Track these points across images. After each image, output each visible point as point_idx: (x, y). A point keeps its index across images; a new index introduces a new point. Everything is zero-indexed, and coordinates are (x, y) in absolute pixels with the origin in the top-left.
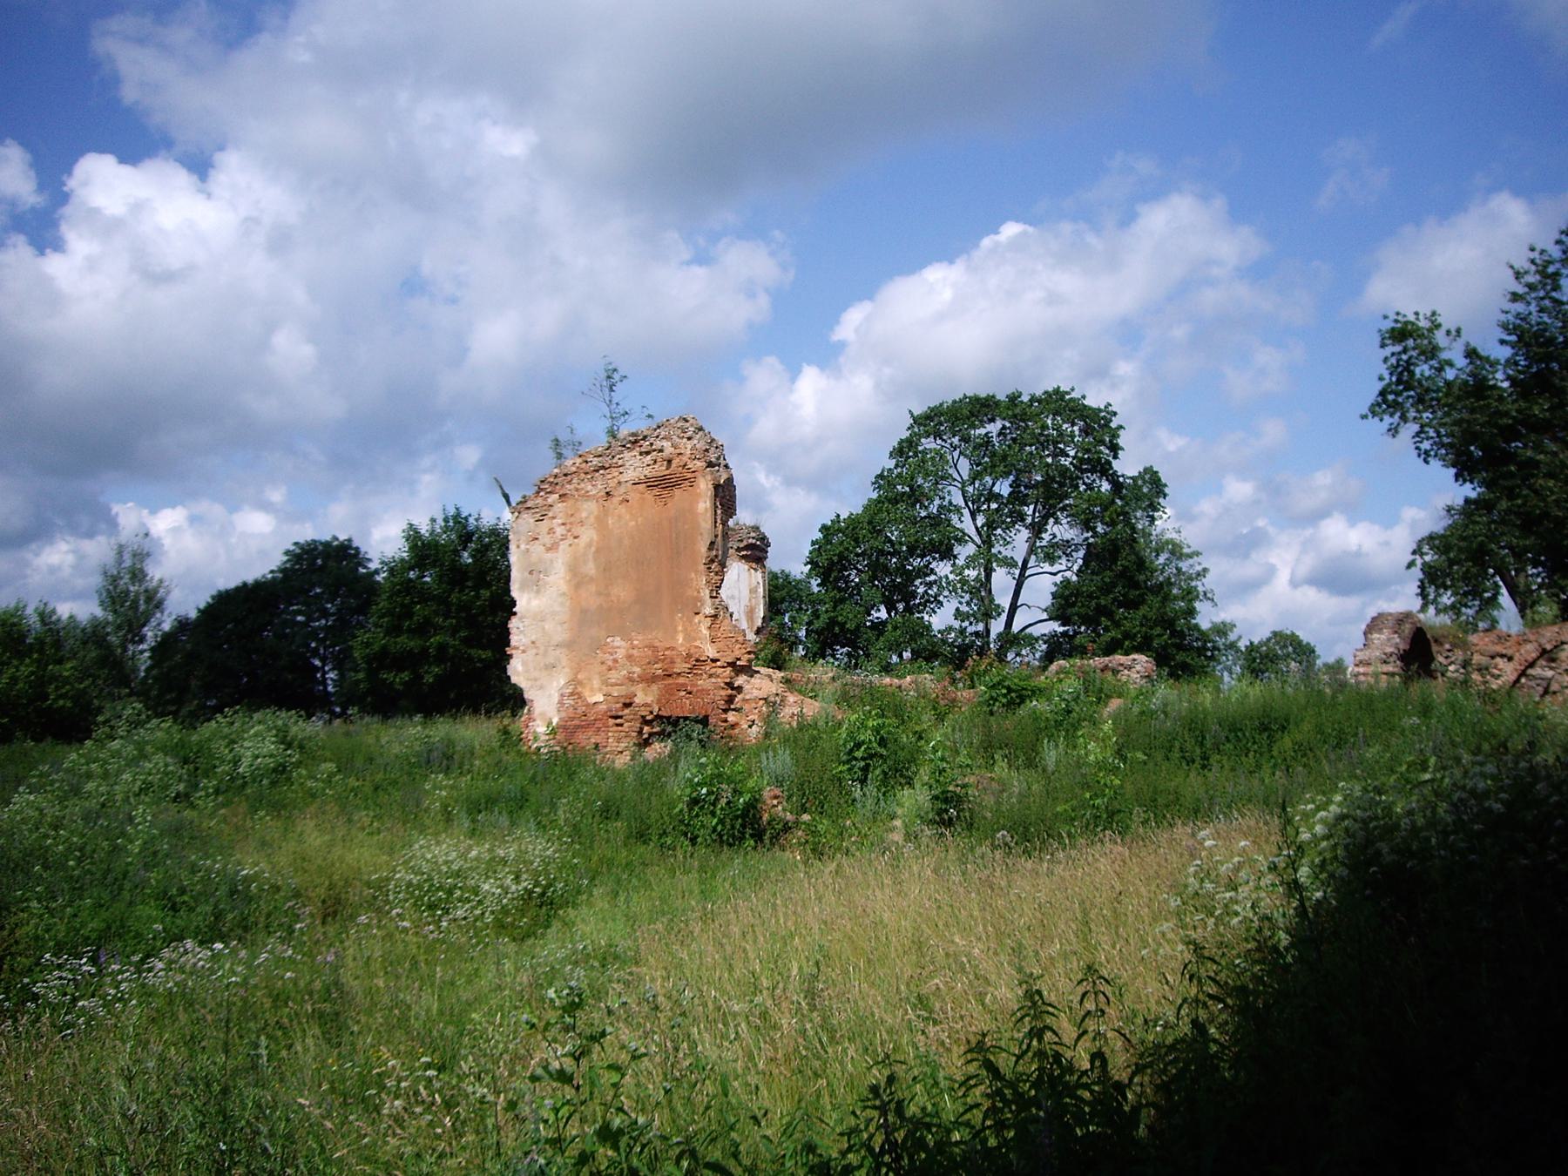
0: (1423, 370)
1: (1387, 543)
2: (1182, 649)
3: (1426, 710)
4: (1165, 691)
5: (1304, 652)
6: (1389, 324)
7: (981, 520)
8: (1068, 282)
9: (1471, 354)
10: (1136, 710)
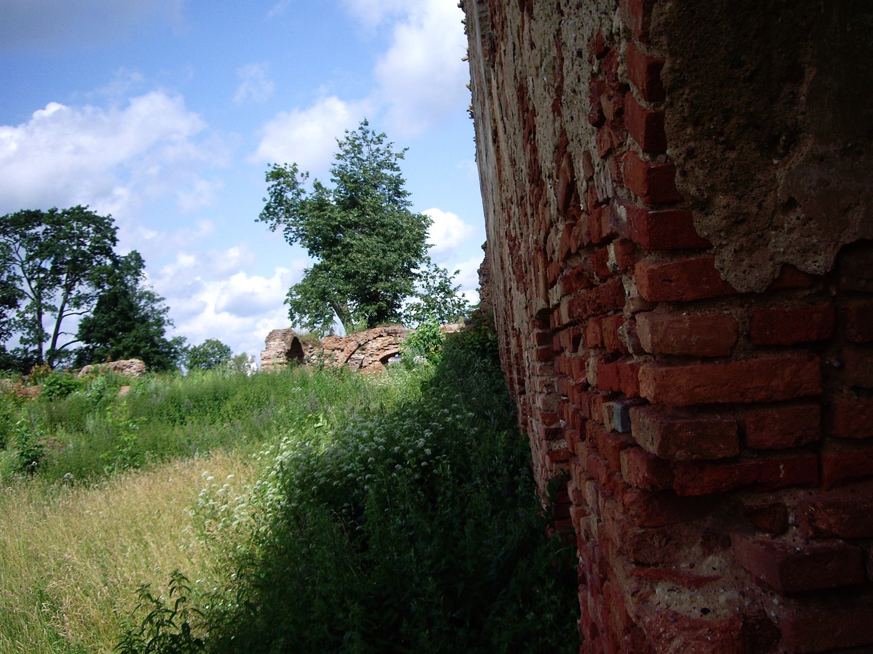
0: (289, 195)
1: (269, 287)
2: (159, 356)
3: (304, 383)
4: (156, 381)
5: (225, 351)
6: (270, 170)
7: (34, 284)
8: (86, 140)
9: (318, 186)
10: (139, 392)
